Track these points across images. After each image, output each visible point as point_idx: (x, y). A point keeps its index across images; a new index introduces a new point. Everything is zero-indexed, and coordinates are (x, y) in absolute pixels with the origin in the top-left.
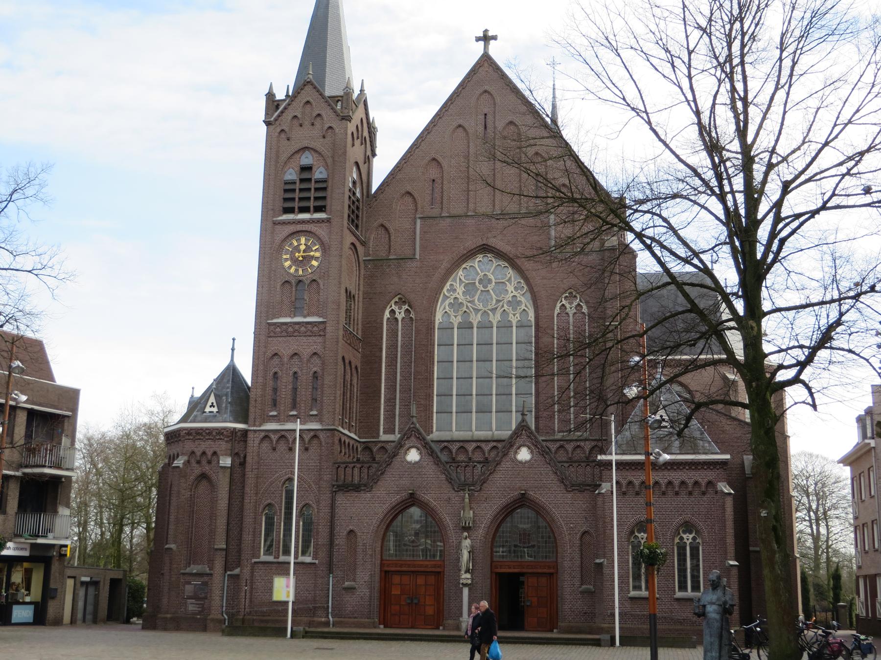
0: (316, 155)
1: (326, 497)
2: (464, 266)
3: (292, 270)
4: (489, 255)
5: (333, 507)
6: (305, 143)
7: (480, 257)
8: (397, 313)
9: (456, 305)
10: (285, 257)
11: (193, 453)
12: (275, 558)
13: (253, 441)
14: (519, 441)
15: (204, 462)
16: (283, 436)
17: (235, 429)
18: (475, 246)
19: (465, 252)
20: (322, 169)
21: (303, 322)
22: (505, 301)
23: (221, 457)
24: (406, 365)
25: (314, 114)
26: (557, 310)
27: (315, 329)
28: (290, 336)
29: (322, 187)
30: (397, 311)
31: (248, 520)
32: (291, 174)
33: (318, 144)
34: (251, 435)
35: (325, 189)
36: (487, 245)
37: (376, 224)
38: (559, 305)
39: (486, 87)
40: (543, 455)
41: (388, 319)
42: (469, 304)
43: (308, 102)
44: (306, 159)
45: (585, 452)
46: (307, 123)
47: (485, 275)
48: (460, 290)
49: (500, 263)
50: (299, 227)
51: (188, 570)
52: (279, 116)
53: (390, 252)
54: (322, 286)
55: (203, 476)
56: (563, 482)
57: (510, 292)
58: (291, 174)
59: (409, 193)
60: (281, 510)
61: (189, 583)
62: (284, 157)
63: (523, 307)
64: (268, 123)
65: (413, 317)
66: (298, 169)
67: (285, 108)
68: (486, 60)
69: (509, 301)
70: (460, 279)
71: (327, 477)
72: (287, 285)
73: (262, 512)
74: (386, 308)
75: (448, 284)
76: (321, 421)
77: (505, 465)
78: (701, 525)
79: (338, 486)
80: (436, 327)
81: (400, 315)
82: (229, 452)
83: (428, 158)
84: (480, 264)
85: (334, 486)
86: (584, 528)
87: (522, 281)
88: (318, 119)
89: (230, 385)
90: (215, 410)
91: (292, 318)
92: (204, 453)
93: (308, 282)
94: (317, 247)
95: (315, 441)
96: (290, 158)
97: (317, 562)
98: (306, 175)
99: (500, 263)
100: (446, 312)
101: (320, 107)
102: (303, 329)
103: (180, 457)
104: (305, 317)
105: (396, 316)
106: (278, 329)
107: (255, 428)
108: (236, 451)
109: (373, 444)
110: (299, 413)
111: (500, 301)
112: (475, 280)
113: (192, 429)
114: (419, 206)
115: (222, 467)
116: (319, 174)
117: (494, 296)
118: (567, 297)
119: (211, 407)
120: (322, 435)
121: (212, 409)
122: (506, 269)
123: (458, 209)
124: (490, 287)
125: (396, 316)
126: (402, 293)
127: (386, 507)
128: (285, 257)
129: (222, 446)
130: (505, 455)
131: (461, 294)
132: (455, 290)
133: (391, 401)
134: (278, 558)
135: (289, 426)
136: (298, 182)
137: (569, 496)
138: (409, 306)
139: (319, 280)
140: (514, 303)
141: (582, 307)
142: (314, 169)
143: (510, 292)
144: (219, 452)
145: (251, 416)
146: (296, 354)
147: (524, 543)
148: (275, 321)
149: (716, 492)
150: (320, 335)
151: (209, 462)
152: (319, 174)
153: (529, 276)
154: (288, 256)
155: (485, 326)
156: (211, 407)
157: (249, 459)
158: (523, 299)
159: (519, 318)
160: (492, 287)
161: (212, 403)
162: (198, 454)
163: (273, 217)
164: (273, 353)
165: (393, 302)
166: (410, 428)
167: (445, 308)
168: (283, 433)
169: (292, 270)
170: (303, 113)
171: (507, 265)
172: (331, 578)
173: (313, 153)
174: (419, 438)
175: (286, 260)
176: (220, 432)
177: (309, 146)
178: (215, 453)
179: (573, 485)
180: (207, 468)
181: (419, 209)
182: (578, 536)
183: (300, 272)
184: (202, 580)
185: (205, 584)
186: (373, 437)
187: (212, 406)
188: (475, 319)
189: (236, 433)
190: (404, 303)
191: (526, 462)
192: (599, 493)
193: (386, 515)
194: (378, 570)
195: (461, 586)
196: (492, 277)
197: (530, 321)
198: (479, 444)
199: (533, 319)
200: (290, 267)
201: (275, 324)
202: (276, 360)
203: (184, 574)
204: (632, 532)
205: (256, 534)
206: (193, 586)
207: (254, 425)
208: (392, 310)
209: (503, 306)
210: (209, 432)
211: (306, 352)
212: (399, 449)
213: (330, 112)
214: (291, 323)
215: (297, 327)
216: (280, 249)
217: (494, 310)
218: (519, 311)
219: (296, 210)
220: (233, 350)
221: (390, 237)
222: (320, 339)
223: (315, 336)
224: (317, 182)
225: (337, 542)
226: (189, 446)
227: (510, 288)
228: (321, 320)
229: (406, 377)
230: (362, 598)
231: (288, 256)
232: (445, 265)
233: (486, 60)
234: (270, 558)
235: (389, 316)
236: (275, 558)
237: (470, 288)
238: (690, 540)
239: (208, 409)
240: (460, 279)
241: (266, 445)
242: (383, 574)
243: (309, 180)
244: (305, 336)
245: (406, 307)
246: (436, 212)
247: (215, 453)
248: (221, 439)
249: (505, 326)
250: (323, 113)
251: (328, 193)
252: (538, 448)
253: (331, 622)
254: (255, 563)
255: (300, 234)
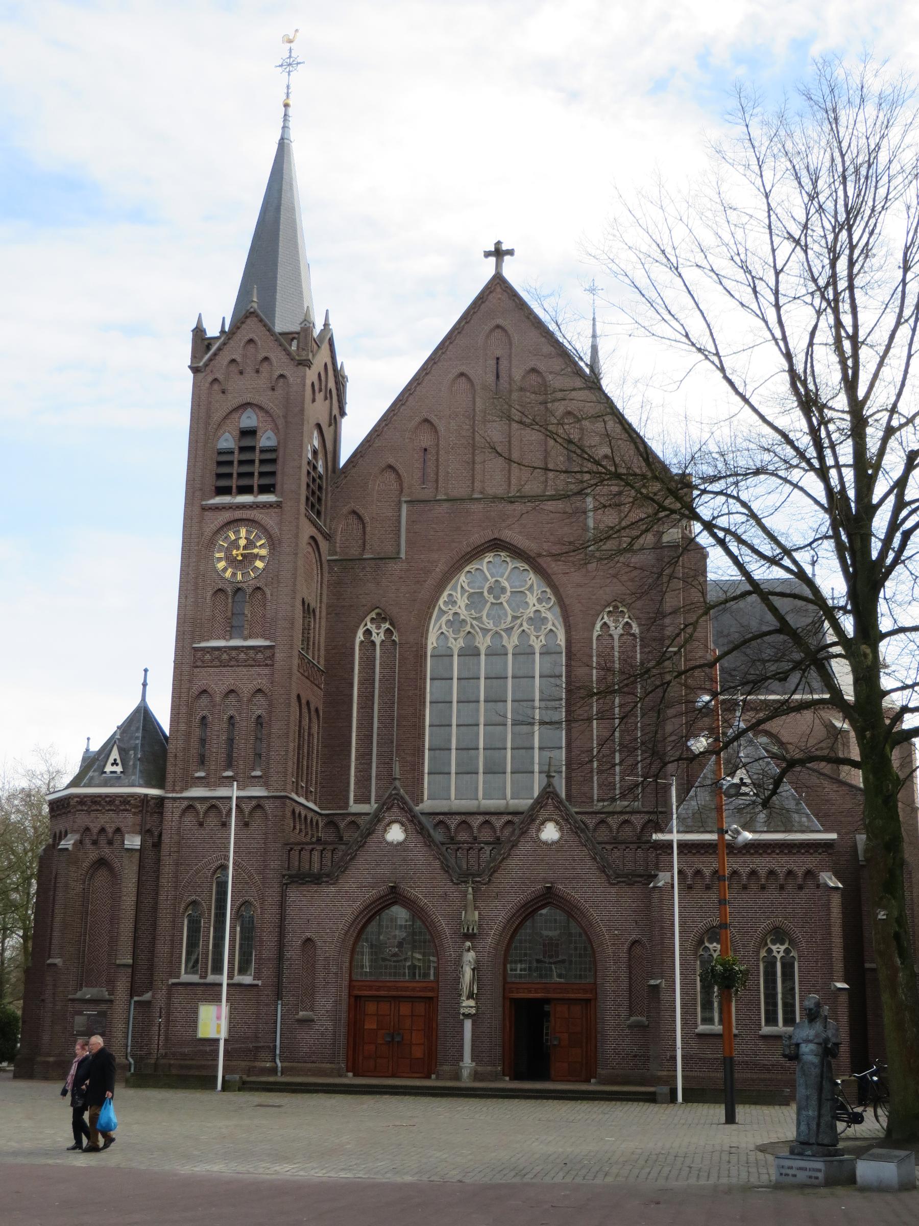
0: (261, 414)
1: (273, 894)
2: (467, 569)
3: (228, 574)
4: (502, 554)
5: (282, 905)
6: (247, 398)
7: (489, 557)
8: (374, 634)
9: (456, 623)
10: (217, 555)
11: (87, 829)
12: (201, 977)
13: (172, 813)
14: (543, 814)
15: (103, 841)
16: (213, 807)
17: (146, 795)
18: (483, 541)
19: (469, 549)
20: (270, 433)
21: (243, 647)
22: (525, 617)
23: (127, 836)
24: (387, 706)
25: (260, 357)
26: (360, 636)
27: (260, 656)
28: (224, 666)
29: (271, 457)
30: (374, 631)
31: (164, 923)
32: (227, 441)
33: (264, 399)
34: (168, 805)
35: (273, 461)
36: (500, 540)
37: (345, 510)
38: (598, 626)
39: (500, 321)
40: (576, 833)
41: (362, 642)
42: (474, 622)
43: (251, 341)
44: (248, 420)
45: (611, 831)
46: (249, 370)
47: (497, 581)
48: (462, 601)
49: (518, 565)
50: (238, 514)
51: (79, 995)
52: (210, 360)
53: (364, 549)
54: (269, 596)
55: (102, 863)
56: (604, 872)
57: (531, 605)
58: (227, 441)
59: (390, 467)
60: (210, 910)
61: (80, 1013)
62: (217, 417)
63: (550, 626)
64: (195, 370)
65: (397, 639)
66: (236, 433)
67: (219, 349)
68: (498, 283)
69: (530, 618)
70: (462, 587)
71: (274, 864)
72: (220, 594)
73: (184, 913)
74: (358, 627)
75: (445, 594)
76: (266, 785)
77: (524, 847)
78: (797, 933)
79: (290, 876)
80: (429, 654)
81: (378, 637)
82: (138, 828)
83: (418, 419)
84: (491, 566)
85: (284, 876)
86: (634, 937)
87: (548, 590)
88: (265, 364)
89: (139, 734)
90: (119, 769)
91: (227, 640)
92: (103, 830)
93: (249, 591)
94: (262, 542)
95: (258, 813)
96: (225, 418)
97: (259, 983)
98: (247, 442)
99: (518, 565)
100: (442, 633)
101: (267, 348)
102: (242, 656)
103: (69, 836)
104: (245, 639)
105: (373, 638)
106: (208, 657)
107: (174, 795)
108: (148, 827)
109: (341, 817)
110: (237, 774)
111: (517, 617)
112: (483, 588)
113: (86, 796)
114: (405, 485)
115: (128, 849)
116: (266, 439)
117: (509, 611)
118: (610, 612)
119: (113, 764)
120: (268, 806)
121: (115, 768)
122: (525, 573)
123: (459, 489)
124: (503, 599)
125: (373, 638)
126: (381, 606)
127: (358, 905)
128: (217, 555)
129: (129, 819)
130: (524, 833)
131: (463, 607)
132: (455, 602)
133: (365, 757)
134: (205, 977)
135: (222, 792)
136: (236, 452)
137: (613, 890)
138: (391, 624)
139: (265, 588)
140: (537, 620)
141: (631, 627)
142: (259, 433)
143: (531, 605)
144: (123, 829)
145: (170, 778)
146: (232, 691)
147: (551, 957)
148: (203, 644)
149: (818, 886)
150: (267, 665)
151: (110, 843)
152: (266, 439)
153: (557, 584)
154: (222, 555)
155: (497, 653)
156: (113, 764)
157: (166, 838)
158: (549, 615)
159: (544, 642)
160: (507, 598)
161: (115, 760)
162: (95, 831)
163: (203, 500)
164: (200, 690)
165: (368, 619)
166: (391, 795)
167: (440, 628)
168: (214, 802)
169: (228, 574)
170: (244, 356)
171: (527, 567)
172: (279, 1006)
173: (257, 410)
174: (403, 809)
175: (220, 559)
176: (125, 800)
177: (252, 401)
178: (118, 830)
179: (618, 876)
180: (106, 851)
181: (406, 491)
182: (626, 947)
183: (239, 577)
184: (99, 1008)
185: (103, 1014)
186: (340, 808)
187: (115, 763)
188: (483, 643)
189: (148, 801)
190: (384, 620)
191: (553, 843)
192: (654, 887)
193: (357, 917)
194: (345, 994)
195: (461, 1017)
196: (506, 584)
197: (560, 645)
198: (487, 817)
199: (563, 643)
200: (225, 570)
201: (203, 649)
202: (204, 700)
203: (73, 1000)
204: (701, 942)
205: (175, 943)
206: (85, 1017)
207: (173, 791)
208: (368, 630)
209: (521, 625)
210: (110, 800)
211: (246, 689)
212: (376, 825)
213: (282, 355)
214: (225, 647)
215: (234, 653)
216: (211, 544)
217: (509, 630)
218: (543, 632)
219: (234, 490)
220: (145, 685)
221: (364, 527)
222: (266, 671)
223: (259, 666)
224: (263, 451)
225: (288, 955)
226: (82, 820)
227: (532, 599)
228: (267, 643)
229: (386, 723)
230: (322, 1034)
231: (222, 555)
232: (440, 568)
233: (498, 283)
234: (195, 978)
235: (362, 638)
236: (201, 977)
237: (475, 600)
238: (782, 954)
239: (109, 768)
240: (462, 587)
241: (189, 819)
242: (353, 1000)
243: (252, 449)
244: (245, 666)
245: (387, 625)
246: (428, 494)
247: (118, 830)
248: (127, 810)
249: (523, 652)
250: (272, 356)
251: (279, 468)
252: (570, 823)
253: (279, 1069)
254: (174, 984)
255: (239, 523)
